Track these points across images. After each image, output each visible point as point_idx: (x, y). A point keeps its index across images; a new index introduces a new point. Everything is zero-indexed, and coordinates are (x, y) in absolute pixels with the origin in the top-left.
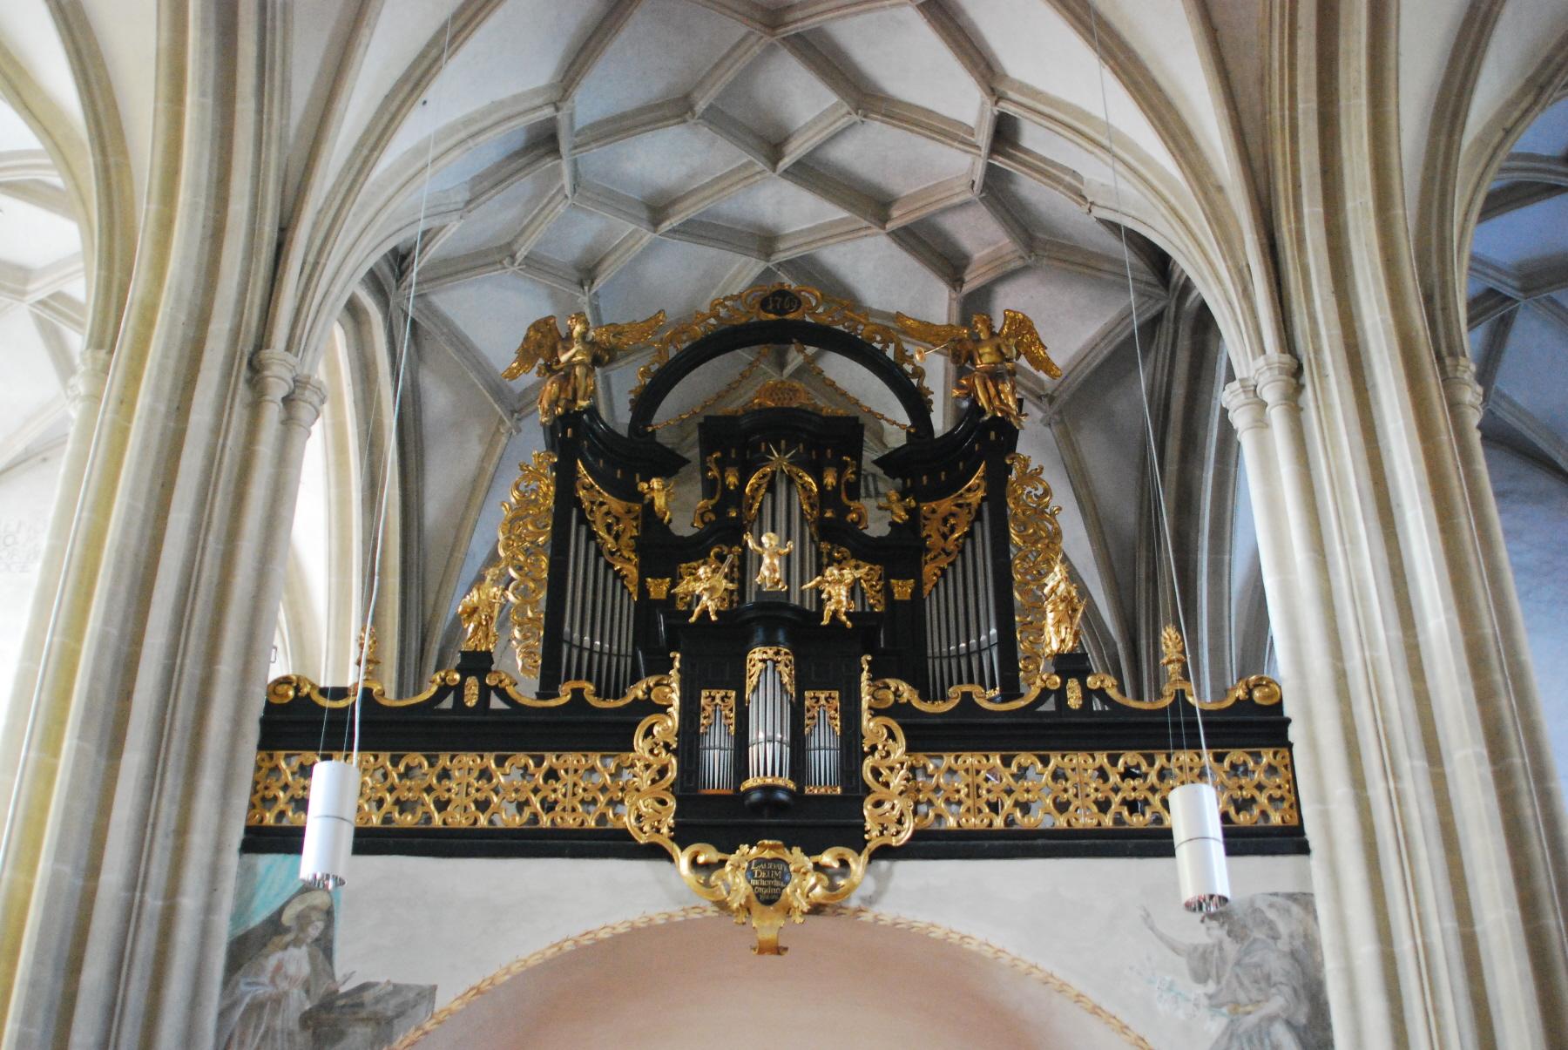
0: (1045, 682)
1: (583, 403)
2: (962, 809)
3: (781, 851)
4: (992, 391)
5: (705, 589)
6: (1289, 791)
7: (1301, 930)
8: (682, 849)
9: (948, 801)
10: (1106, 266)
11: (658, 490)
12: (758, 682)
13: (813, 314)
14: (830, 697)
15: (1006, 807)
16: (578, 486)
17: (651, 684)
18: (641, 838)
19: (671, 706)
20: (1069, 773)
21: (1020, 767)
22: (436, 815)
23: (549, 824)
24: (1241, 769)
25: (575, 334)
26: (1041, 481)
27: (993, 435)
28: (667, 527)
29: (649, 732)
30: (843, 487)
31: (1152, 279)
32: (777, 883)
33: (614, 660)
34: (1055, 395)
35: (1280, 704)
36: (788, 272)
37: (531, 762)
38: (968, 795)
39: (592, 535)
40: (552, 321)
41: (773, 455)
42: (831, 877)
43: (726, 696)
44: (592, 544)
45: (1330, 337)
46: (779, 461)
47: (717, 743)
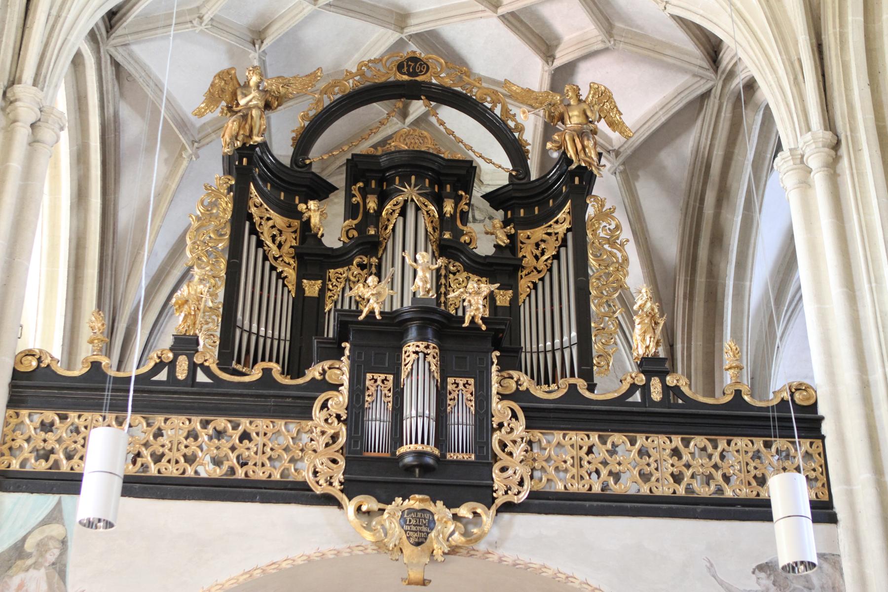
0: (634, 379)
1: (257, 139)
2: (569, 476)
3: (428, 503)
4: (579, 146)
5: (372, 295)
6: (822, 473)
7: (830, 583)
8: (350, 499)
9: (557, 469)
10: (668, 52)
11: (314, 211)
12: (412, 369)
13: (437, 77)
14: (467, 383)
15: (602, 476)
16: (251, 203)
17: (326, 368)
18: (317, 489)
19: (342, 385)
20: (651, 451)
21: (614, 445)
22: (152, 465)
23: (243, 476)
24: (784, 454)
25: (252, 83)
26: (613, 218)
27: (577, 180)
28: (320, 240)
29: (324, 406)
30: (458, 215)
31: (705, 64)
32: (424, 529)
33: (276, 343)
34: (621, 150)
35: (815, 404)
36: (416, 43)
37: (229, 426)
38: (573, 465)
39: (260, 244)
40: (233, 72)
41: (406, 188)
42: (465, 526)
43: (386, 379)
44: (260, 251)
45: (865, 120)
46: (410, 192)
47: (378, 416)
